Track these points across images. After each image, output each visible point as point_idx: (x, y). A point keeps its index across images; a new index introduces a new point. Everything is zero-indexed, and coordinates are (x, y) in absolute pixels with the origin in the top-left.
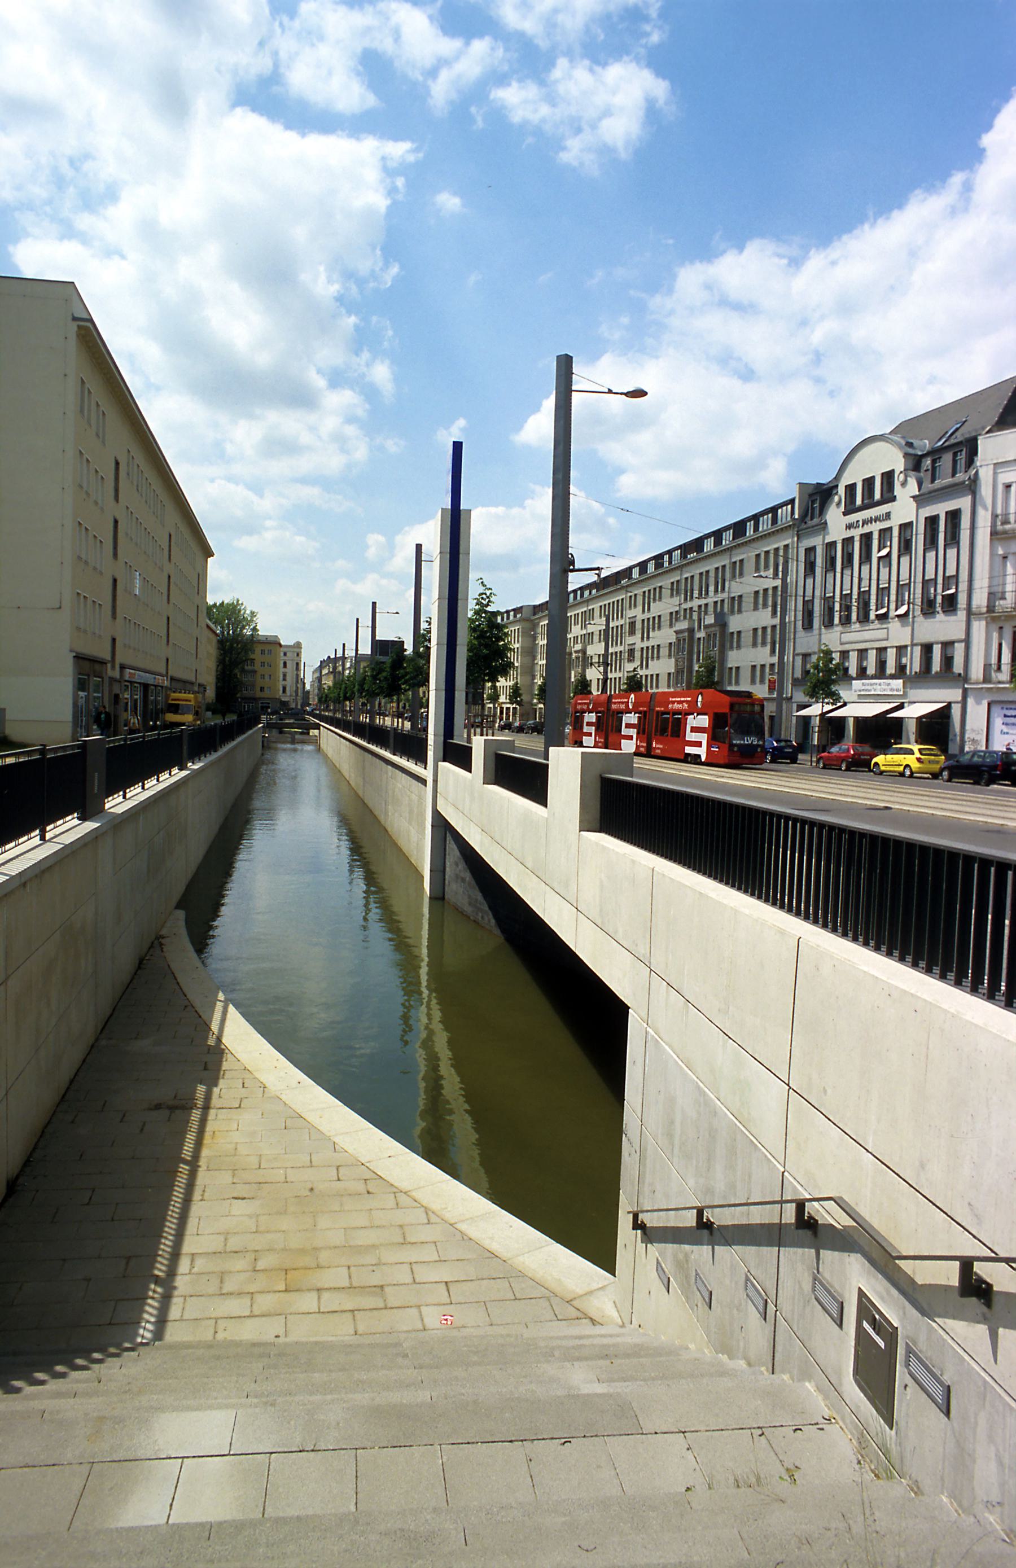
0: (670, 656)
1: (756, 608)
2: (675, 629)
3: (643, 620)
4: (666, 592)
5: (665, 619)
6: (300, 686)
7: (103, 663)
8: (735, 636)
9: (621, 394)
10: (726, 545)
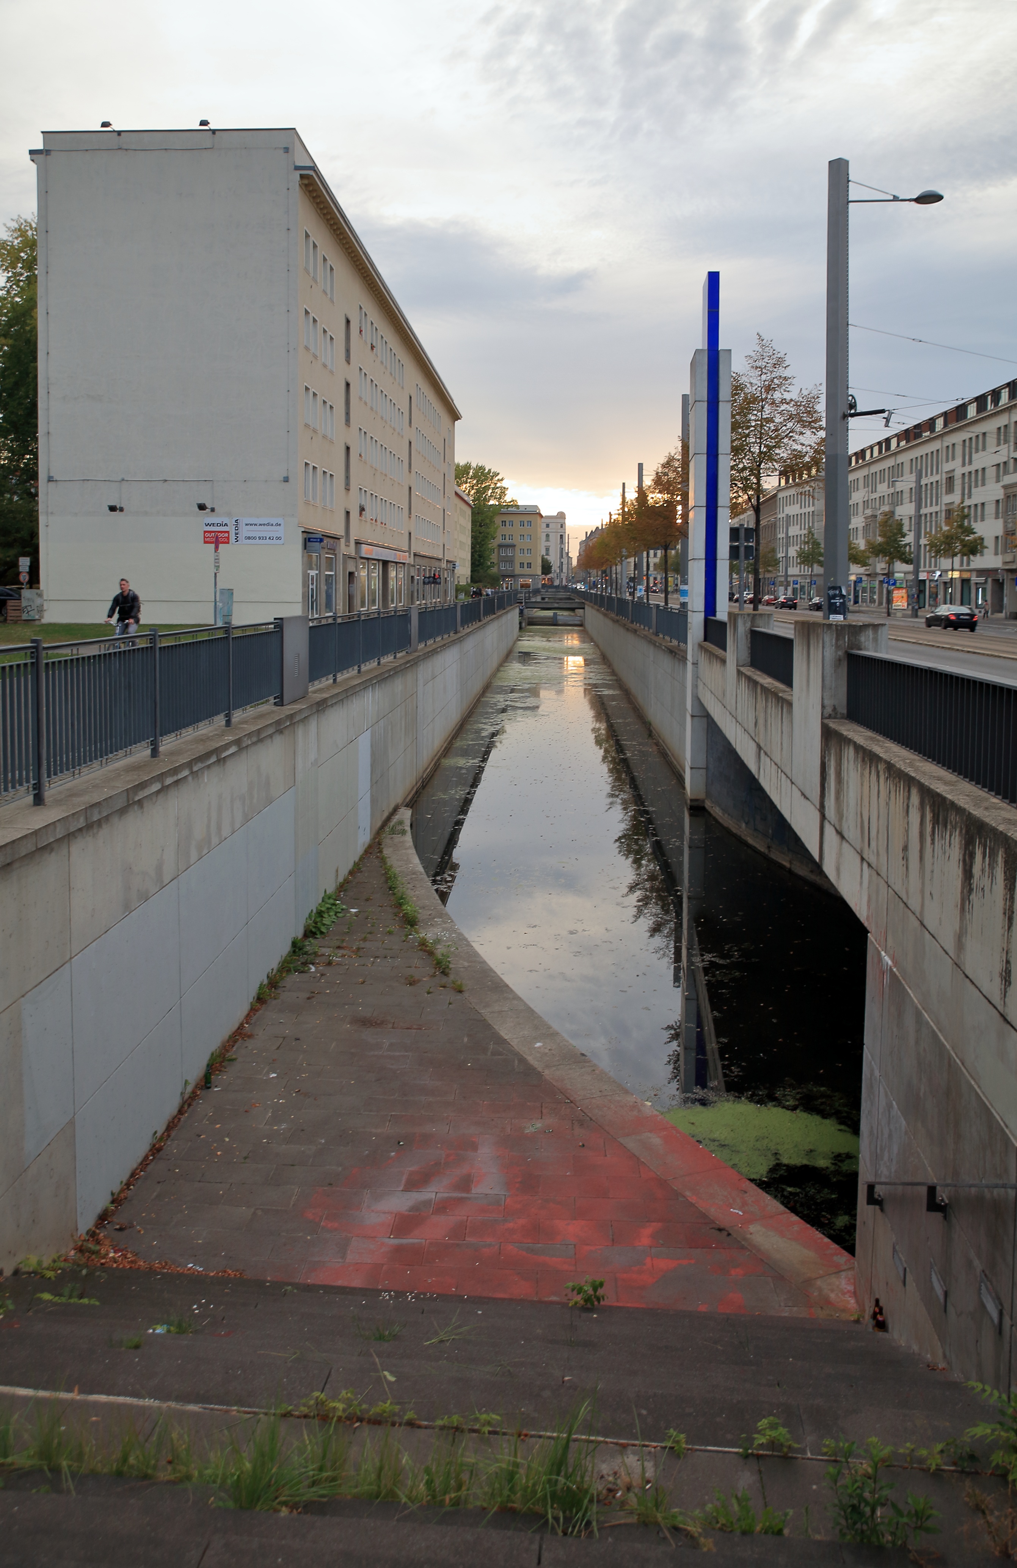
0: (997, 517)
2: (1001, 484)
4: (991, 440)
6: (565, 561)
9: (910, 200)
10: (991, 410)
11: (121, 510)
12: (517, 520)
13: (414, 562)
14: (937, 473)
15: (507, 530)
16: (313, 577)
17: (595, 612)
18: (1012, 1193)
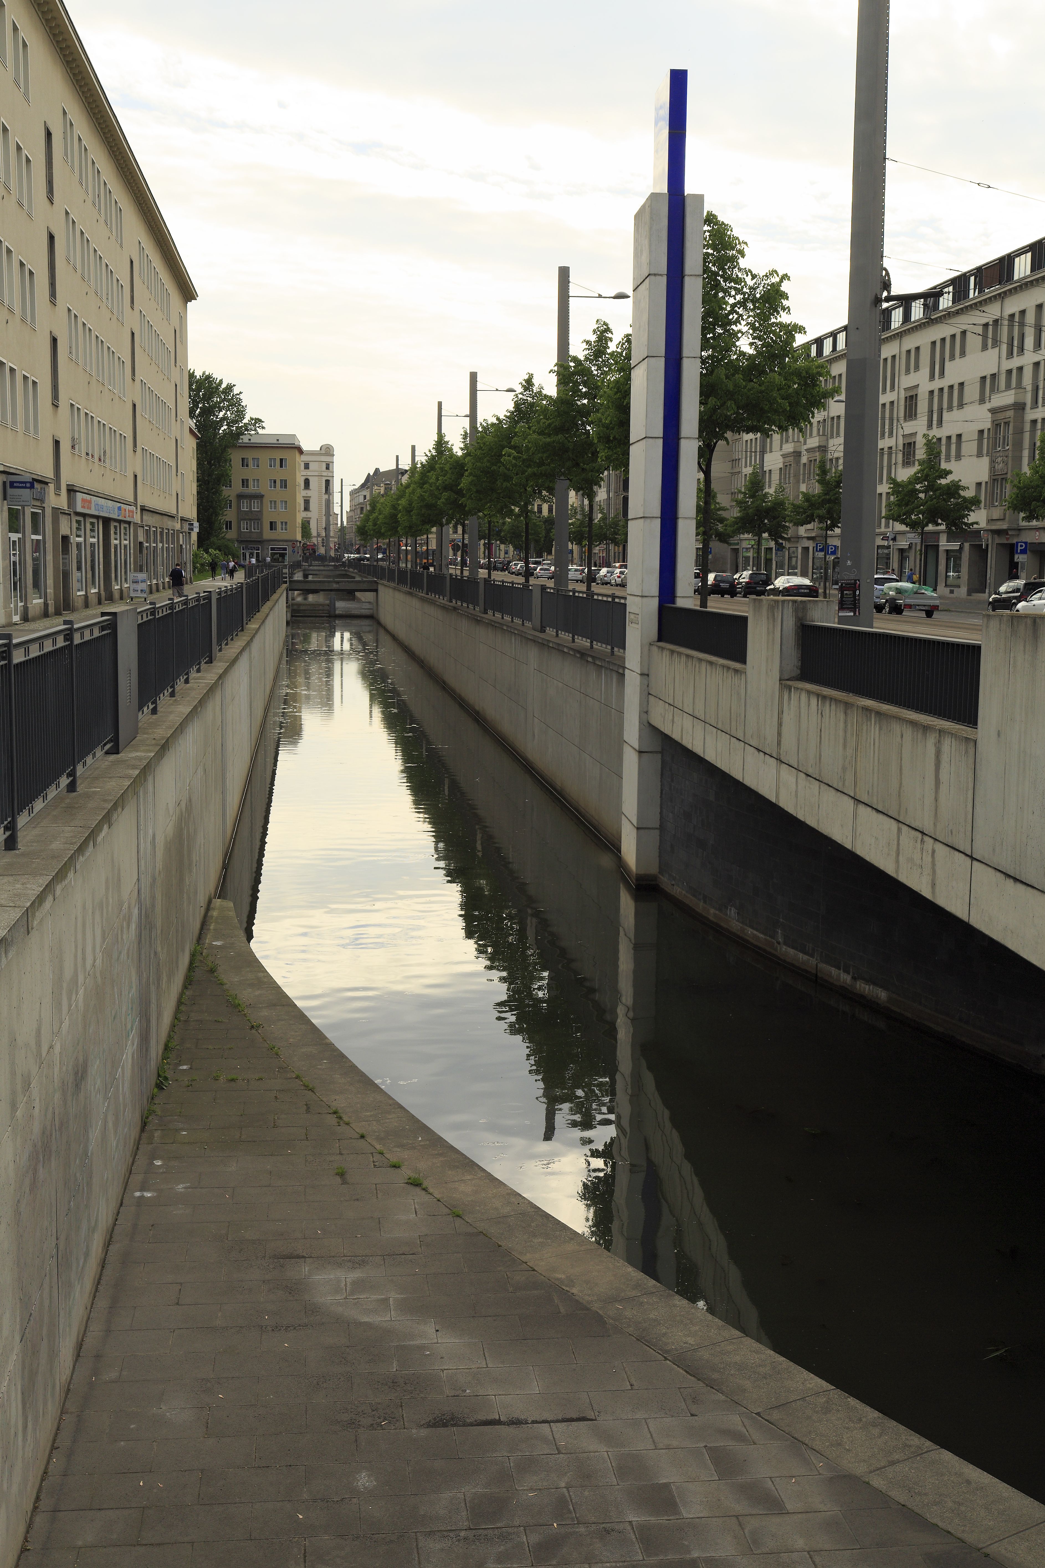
0: (979, 455)
2: (988, 406)
4: (974, 342)
5: (972, 392)
7: (35, 483)
8: (835, 419)
10: (974, 298)
12: (264, 457)
15: (249, 473)
16: (14, 542)
17: (400, 596)
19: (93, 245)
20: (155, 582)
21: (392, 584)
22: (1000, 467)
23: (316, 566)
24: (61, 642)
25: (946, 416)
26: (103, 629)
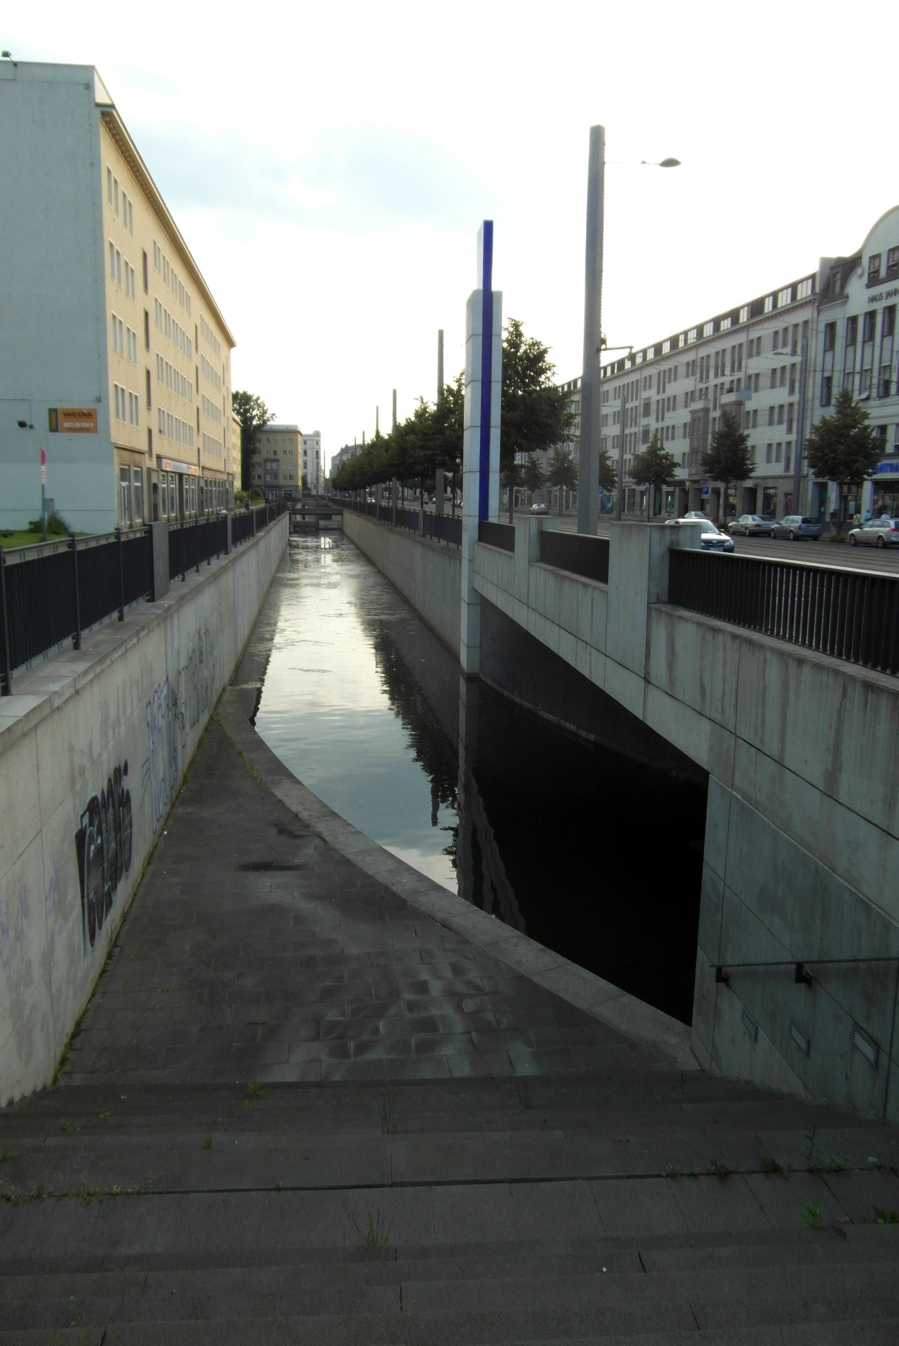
0: (685, 437)
1: (773, 386)
2: (689, 409)
3: (658, 401)
5: (681, 400)
8: (751, 415)
11: (31, 427)
13: (203, 474)
14: (637, 399)
16: (124, 487)
18: (894, 964)
19: (126, 325)
20: (211, 509)
21: (350, 511)
22: (695, 444)
23: (309, 501)
24: (112, 540)
25: (666, 415)
26: (145, 533)
